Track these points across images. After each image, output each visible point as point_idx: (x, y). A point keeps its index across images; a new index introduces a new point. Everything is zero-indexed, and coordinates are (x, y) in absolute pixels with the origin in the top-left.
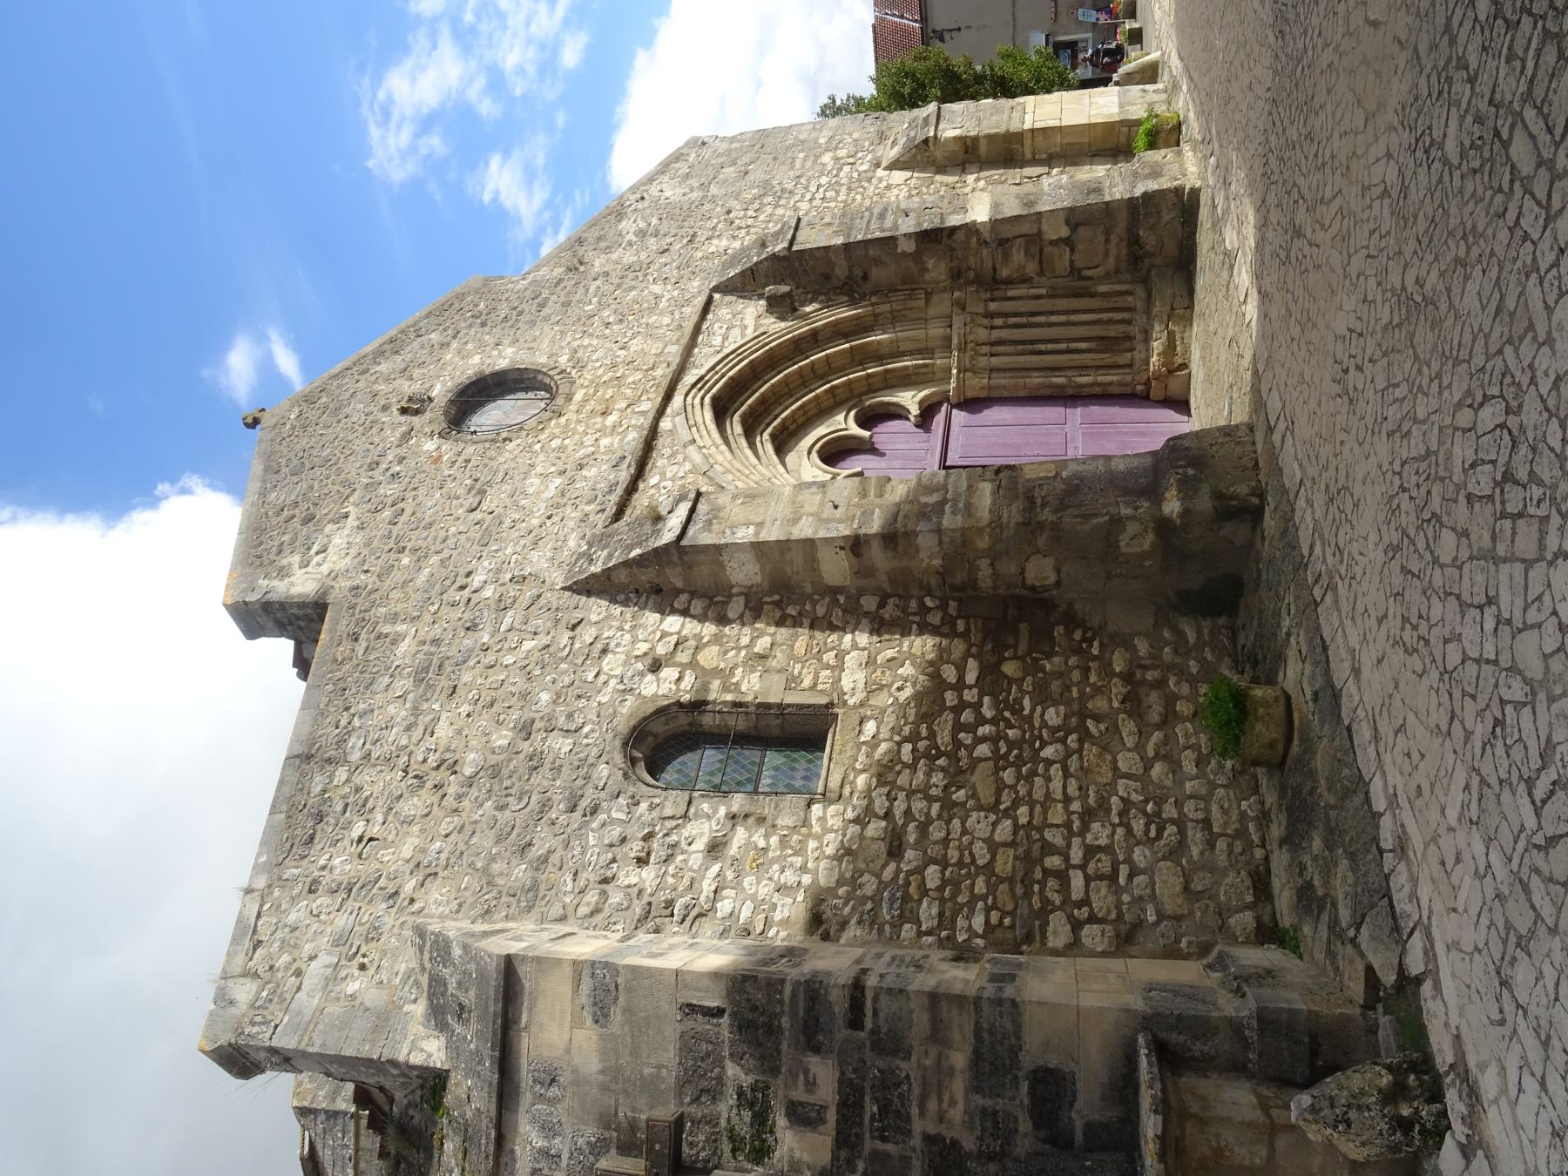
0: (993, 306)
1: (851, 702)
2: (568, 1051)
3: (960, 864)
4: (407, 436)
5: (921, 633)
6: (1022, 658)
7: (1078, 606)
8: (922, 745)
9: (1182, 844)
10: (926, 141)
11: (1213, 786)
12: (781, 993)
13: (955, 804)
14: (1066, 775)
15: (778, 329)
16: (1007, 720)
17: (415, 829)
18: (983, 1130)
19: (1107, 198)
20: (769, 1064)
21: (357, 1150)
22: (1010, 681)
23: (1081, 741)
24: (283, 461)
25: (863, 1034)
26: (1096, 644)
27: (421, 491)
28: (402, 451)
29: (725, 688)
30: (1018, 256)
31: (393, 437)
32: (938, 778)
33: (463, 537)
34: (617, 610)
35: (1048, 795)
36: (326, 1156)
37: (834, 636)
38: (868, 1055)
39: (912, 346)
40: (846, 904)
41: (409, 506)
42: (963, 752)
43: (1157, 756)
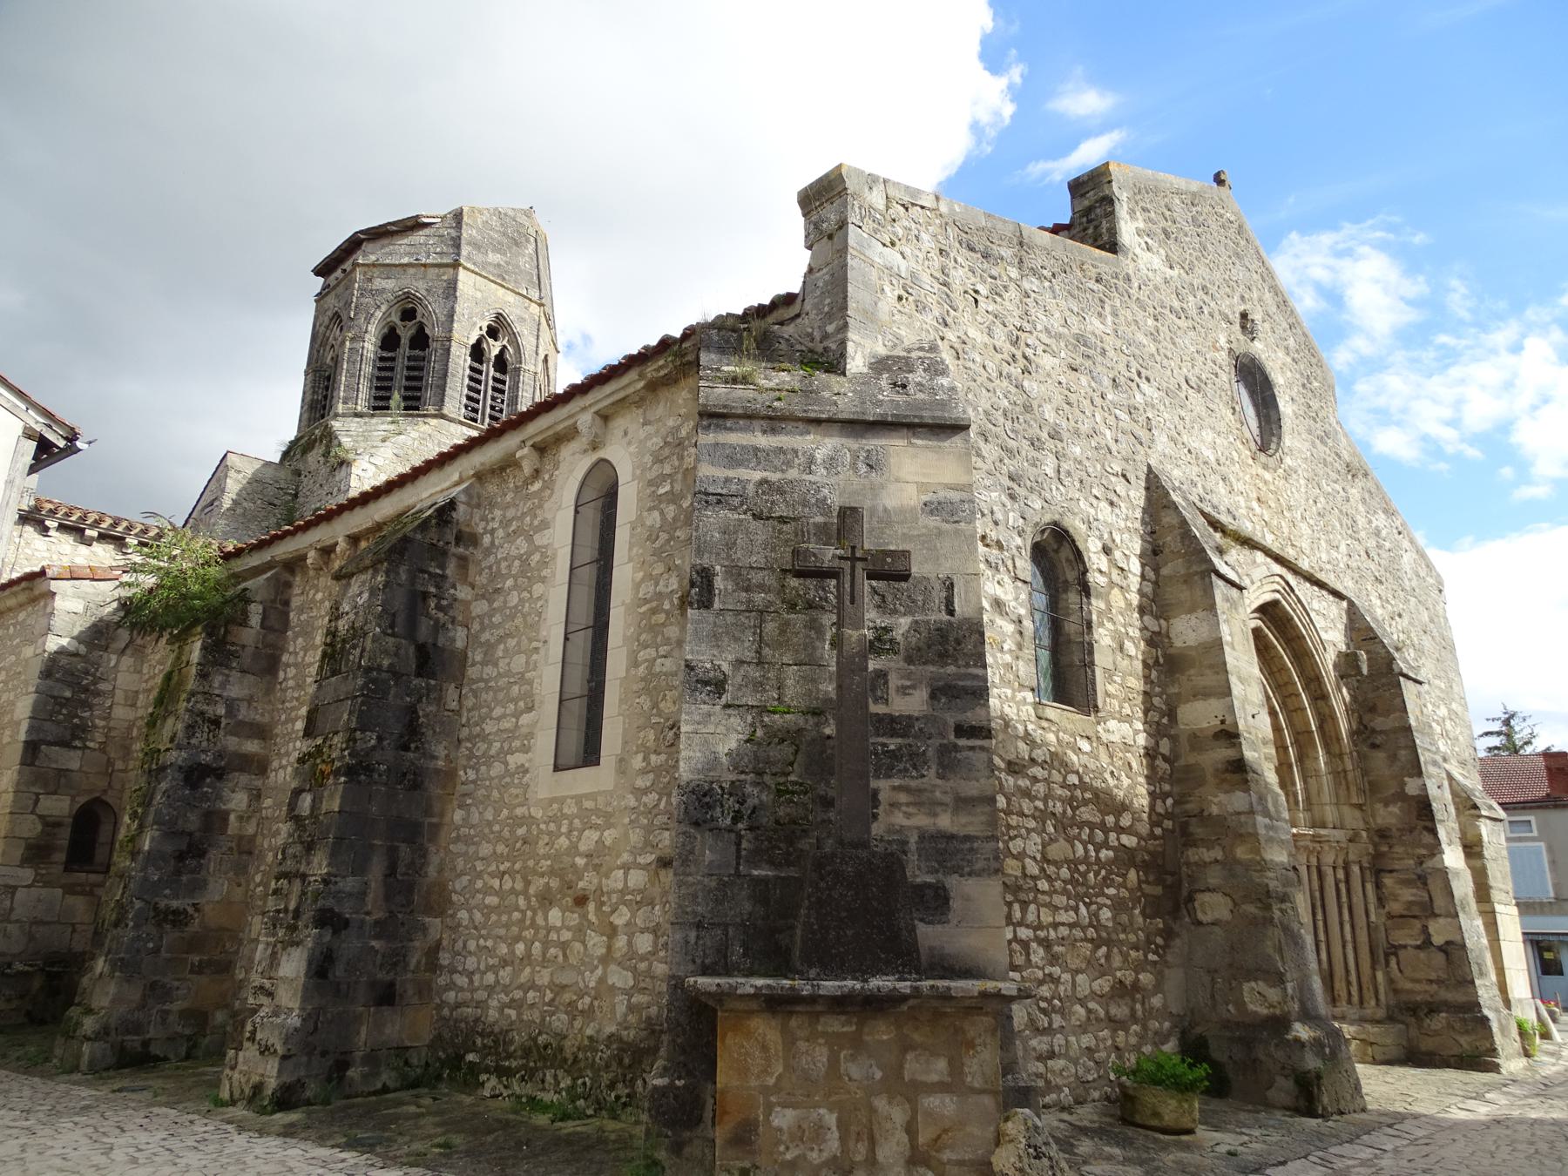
0: (1356, 869)
1: (1099, 728)
2: (897, 480)
3: (1009, 827)
5: (1151, 794)
6: (1140, 888)
8: (1078, 793)
9: (1039, 1031)
10: (1475, 807)
11: (1075, 1062)
12: (975, 666)
14: (1072, 926)
15: (1327, 661)
17: (986, 339)
18: (889, 842)
19: (1477, 982)
20: (914, 656)
21: (425, 265)
22: (1124, 876)
23: (1092, 941)
25: (952, 737)
26: (1155, 958)
27: (1192, 333)
28: (1216, 315)
29: (1100, 613)
30: (1408, 894)
31: (1225, 306)
34: (1138, 514)
35: (1056, 908)
36: (419, 237)
37: (1140, 715)
38: (936, 742)
39: (1314, 791)
41: (1182, 323)
43: (1089, 1011)
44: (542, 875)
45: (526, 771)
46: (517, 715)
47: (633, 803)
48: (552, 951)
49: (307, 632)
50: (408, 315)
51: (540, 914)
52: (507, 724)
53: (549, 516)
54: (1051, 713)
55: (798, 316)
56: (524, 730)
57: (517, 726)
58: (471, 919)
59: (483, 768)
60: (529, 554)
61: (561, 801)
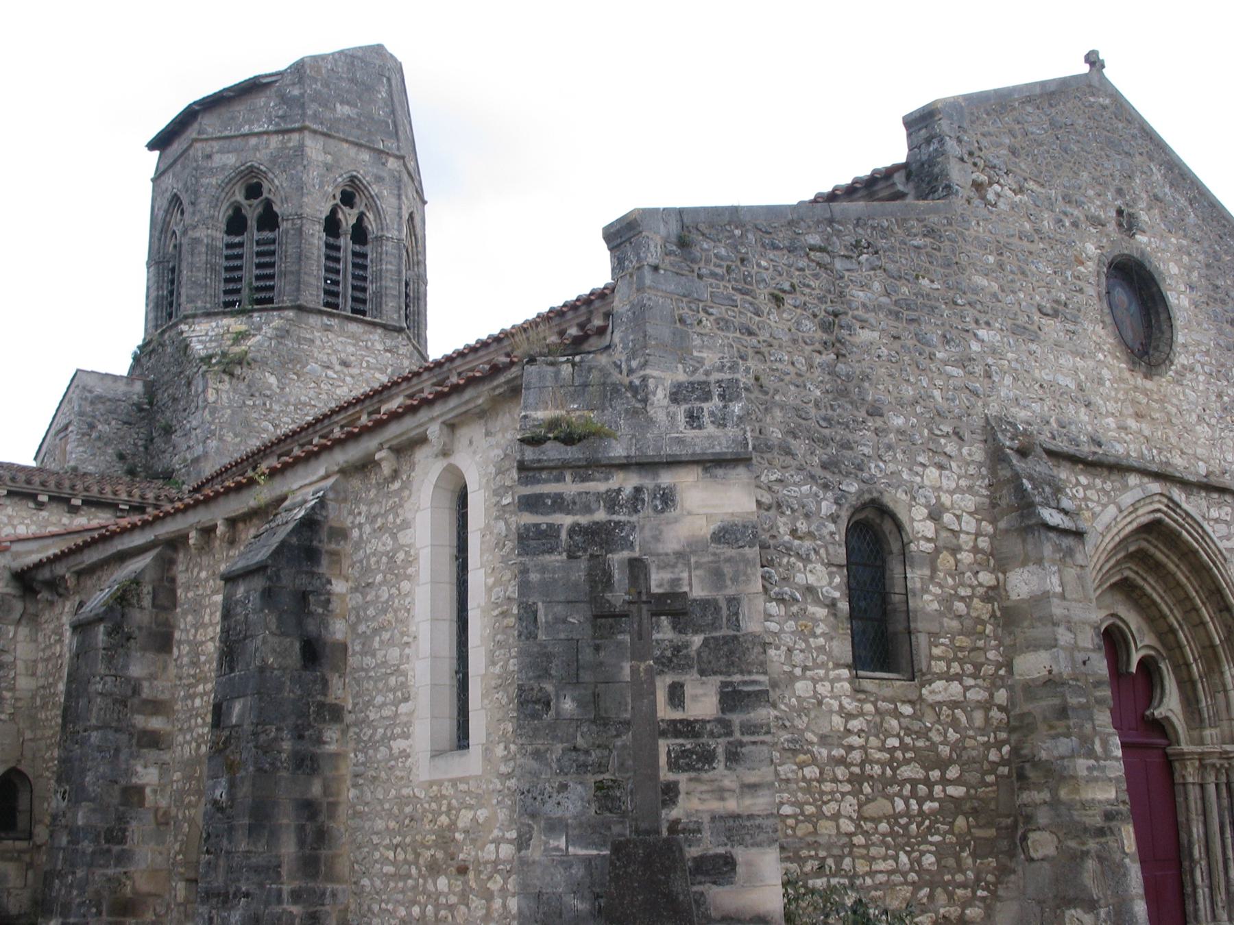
3: (822, 793)
4: (1097, 222)
7: (1013, 877)
8: (899, 754)
13: (861, 785)
14: (890, 873)
16: (923, 823)
22: (952, 824)
23: (914, 883)
24: (1061, 107)
26: (985, 893)
32: (877, 769)
33: (1016, 308)
40: (786, 704)
42: (896, 788)
44: (429, 848)
45: (408, 756)
46: (396, 703)
47: (499, 787)
48: (443, 913)
49: (197, 608)
50: (254, 191)
51: (430, 881)
52: (387, 712)
53: (409, 516)
54: (868, 685)
55: (608, 347)
56: (404, 719)
57: (396, 714)
58: (373, 885)
59: (371, 752)
60: (395, 551)
61: (440, 783)
